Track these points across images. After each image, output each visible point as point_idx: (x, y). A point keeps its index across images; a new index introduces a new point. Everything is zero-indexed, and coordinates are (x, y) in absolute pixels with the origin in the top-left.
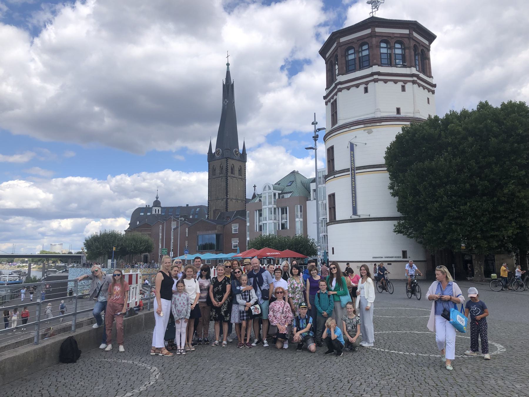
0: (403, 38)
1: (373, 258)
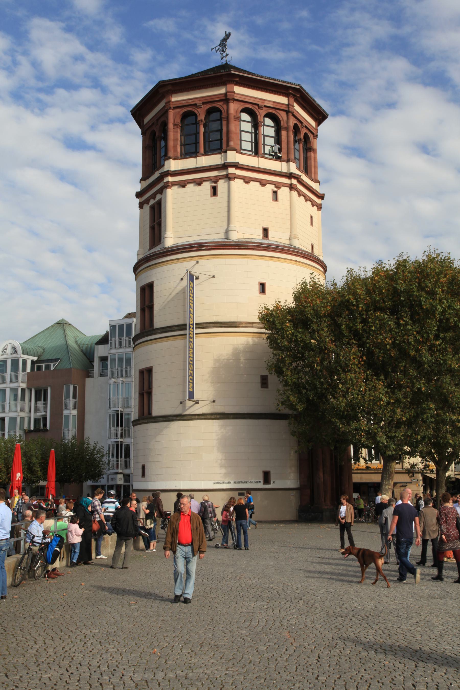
0: (278, 111)
1: (214, 483)
